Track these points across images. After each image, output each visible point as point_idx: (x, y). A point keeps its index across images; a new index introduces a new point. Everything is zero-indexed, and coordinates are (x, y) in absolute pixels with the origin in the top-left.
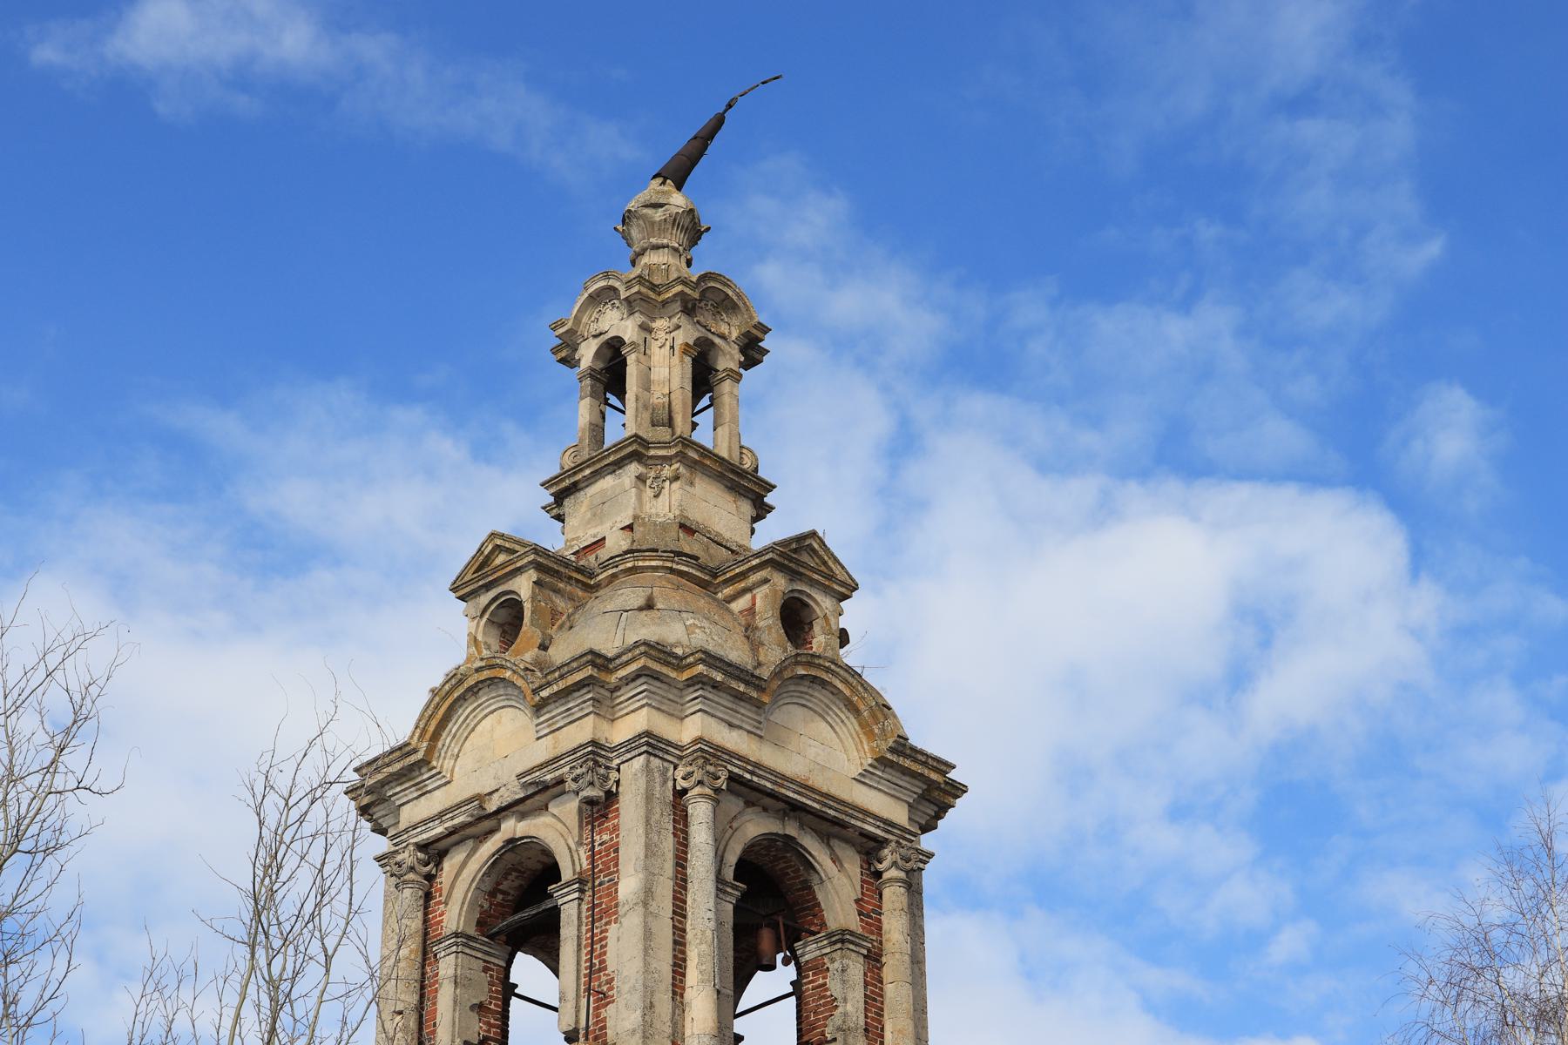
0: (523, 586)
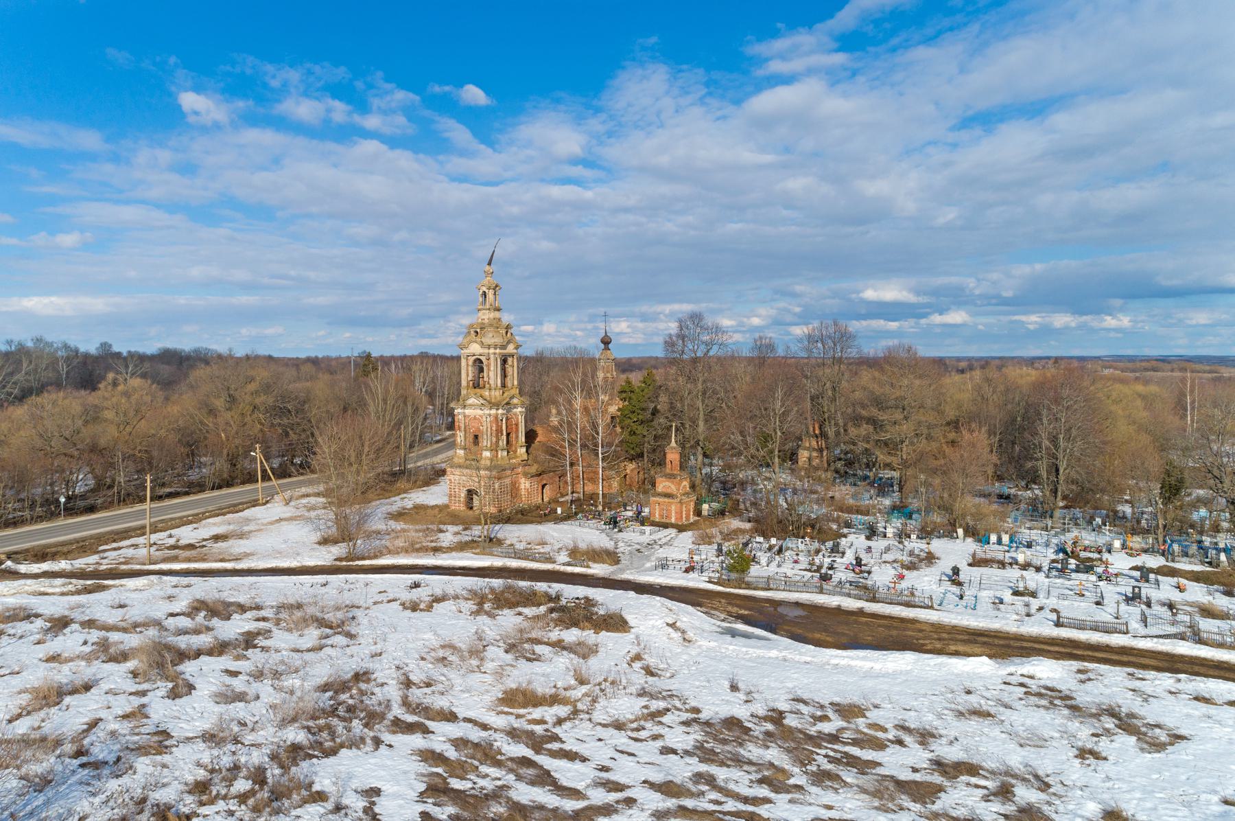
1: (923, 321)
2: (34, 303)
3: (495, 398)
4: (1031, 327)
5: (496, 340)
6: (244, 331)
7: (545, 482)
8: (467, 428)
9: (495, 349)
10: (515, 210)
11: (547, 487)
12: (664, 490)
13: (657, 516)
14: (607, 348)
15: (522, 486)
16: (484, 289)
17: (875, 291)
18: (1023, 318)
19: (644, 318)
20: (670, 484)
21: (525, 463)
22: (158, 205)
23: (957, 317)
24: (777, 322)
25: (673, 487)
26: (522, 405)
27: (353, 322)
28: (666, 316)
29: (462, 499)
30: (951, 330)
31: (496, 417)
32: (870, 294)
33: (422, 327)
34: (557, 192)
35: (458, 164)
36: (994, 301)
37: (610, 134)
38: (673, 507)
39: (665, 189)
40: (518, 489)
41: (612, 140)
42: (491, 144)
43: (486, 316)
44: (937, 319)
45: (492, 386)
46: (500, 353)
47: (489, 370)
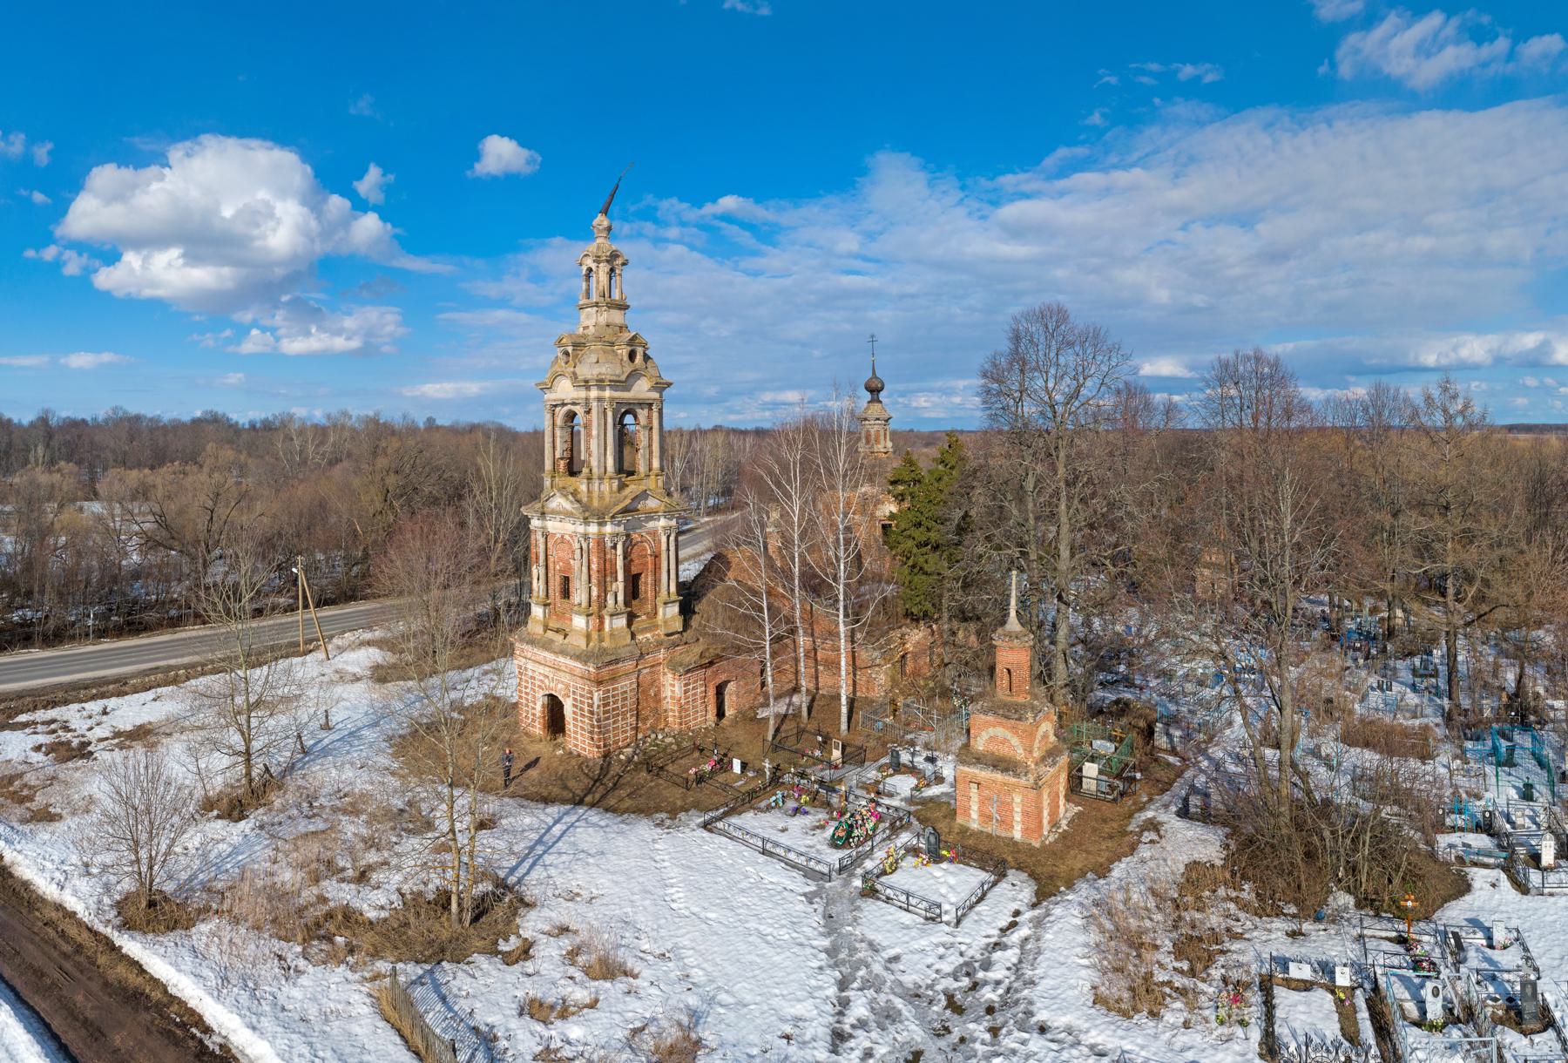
0: (570, 349)
5: (603, 370)
7: (723, 677)
9: (602, 388)
11: (731, 687)
12: (993, 748)
13: (974, 815)
14: (875, 400)
15: (667, 692)
16: (589, 262)
20: (1008, 735)
21: (673, 641)
25: (1015, 741)
29: (538, 714)
31: (600, 541)
38: (1018, 799)
40: (658, 699)
43: (591, 320)
46: (612, 399)
47: (589, 435)
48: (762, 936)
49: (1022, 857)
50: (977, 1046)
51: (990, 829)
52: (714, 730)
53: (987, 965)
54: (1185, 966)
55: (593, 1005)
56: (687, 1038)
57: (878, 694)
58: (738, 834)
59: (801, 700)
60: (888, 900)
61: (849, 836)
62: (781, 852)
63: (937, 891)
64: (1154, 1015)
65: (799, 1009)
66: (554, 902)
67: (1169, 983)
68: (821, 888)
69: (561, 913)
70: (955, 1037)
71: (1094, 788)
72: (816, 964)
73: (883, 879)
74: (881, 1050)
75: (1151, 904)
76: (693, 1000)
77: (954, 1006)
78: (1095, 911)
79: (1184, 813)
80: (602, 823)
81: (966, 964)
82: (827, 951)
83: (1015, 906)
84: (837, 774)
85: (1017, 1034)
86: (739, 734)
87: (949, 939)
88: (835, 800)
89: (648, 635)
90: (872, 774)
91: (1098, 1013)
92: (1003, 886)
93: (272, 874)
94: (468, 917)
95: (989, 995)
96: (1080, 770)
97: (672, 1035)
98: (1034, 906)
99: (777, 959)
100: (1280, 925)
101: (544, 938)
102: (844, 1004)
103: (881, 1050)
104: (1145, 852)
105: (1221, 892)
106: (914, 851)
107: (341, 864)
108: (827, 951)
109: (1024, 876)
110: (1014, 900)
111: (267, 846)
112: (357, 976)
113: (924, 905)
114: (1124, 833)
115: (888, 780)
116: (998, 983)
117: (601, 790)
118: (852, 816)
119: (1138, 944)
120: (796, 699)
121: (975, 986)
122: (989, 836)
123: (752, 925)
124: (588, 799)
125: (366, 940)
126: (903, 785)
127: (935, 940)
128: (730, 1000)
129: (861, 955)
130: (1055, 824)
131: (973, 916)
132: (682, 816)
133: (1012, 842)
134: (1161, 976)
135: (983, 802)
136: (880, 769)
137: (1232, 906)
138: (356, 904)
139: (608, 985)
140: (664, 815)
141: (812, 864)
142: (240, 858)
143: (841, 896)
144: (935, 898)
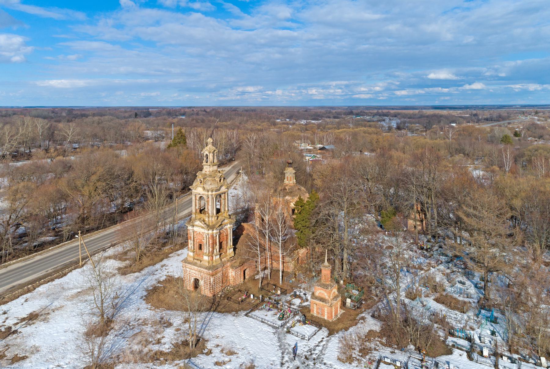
1: (460, 88)
2: (55, 83)
3: (212, 222)
4: (517, 90)
5: (213, 187)
6: (143, 94)
8: (195, 239)
10: (262, 41)
13: (315, 312)
15: (230, 274)
17: (435, 74)
18: (513, 86)
19: (324, 87)
21: (232, 259)
22: (108, 42)
23: (477, 86)
24: (387, 89)
25: (326, 294)
26: (230, 223)
27: (189, 90)
28: (333, 86)
30: (476, 92)
31: (212, 236)
32: (432, 76)
33: (221, 92)
34: (281, 33)
35: (235, 22)
36: (496, 78)
37: (303, 8)
38: (326, 309)
39: (331, 31)
40: (227, 277)
41: (304, 10)
42: (249, 13)
44: (467, 87)
45: (210, 215)
48: (264, 343)
49: (326, 324)
50: (311, 366)
51: (319, 316)
52: (243, 284)
53: (314, 350)
54: (361, 354)
55: (230, 361)
56: (252, 365)
57: (290, 270)
58: (255, 317)
59: (268, 272)
60: (293, 334)
61: (283, 317)
62: (266, 321)
63: (304, 332)
64: (350, 363)
65: (274, 359)
66: (213, 339)
67: (355, 358)
68: (277, 331)
69: (216, 342)
70: (306, 364)
71: (349, 305)
72: (277, 349)
73: (291, 329)
74: (291, 366)
75: (357, 339)
76: (251, 358)
77: (306, 358)
78: (342, 339)
79: (373, 316)
80: (219, 316)
81: (310, 349)
82: (279, 346)
83: (323, 337)
84: (279, 298)
85: (319, 364)
86: (250, 285)
87: (307, 344)
88: (279, 306)
89: (225, 259)
90: (289, 298)
91: (338, 362)
92: (321, 331)
93: (130, 348)
94: (194, 346)
95: (314, 356)
96: (346, 300)
97: (249, 365)
98: (327, 337)
99: (268, 348)
100: (390, 349)
101: (214, 348)
102: (283, 357)
103: (291, 366)
104: (359, 325)
105: (376, 339)
106: (299, 321)
107: (150, 340)
108: (279, 346)
109: (326, 329)
110: (323, 335)
111: (123, 341)
112: (171, 366)
113: (301, 335)
114: (355, 319)
115: (293, 300)
116: (316, 354)
117: (215, 307)
118: (284, 312)
119: (351, 348)
120: (266, 272)
121: (311, 354)
122: (319, 318)
123: (262, 341)
124: (212, 309)
125: (169, 357)
126: (297, 301)
127: (303, 344)
128: (259, 357)
129: (286, 347)
130: (336, 315)
131: (312, 338)
132: (239, 312)
133: (324, 320)
134: (354, 356)
135: (317, 309)
136: (291, 296)
137: (378, 342)
138: (161, 349)
139: (232, 356)
140: (234, 313)
141: (274, 325)
142: (117, 346)
143: (281, 333)
144: (304, 334)
